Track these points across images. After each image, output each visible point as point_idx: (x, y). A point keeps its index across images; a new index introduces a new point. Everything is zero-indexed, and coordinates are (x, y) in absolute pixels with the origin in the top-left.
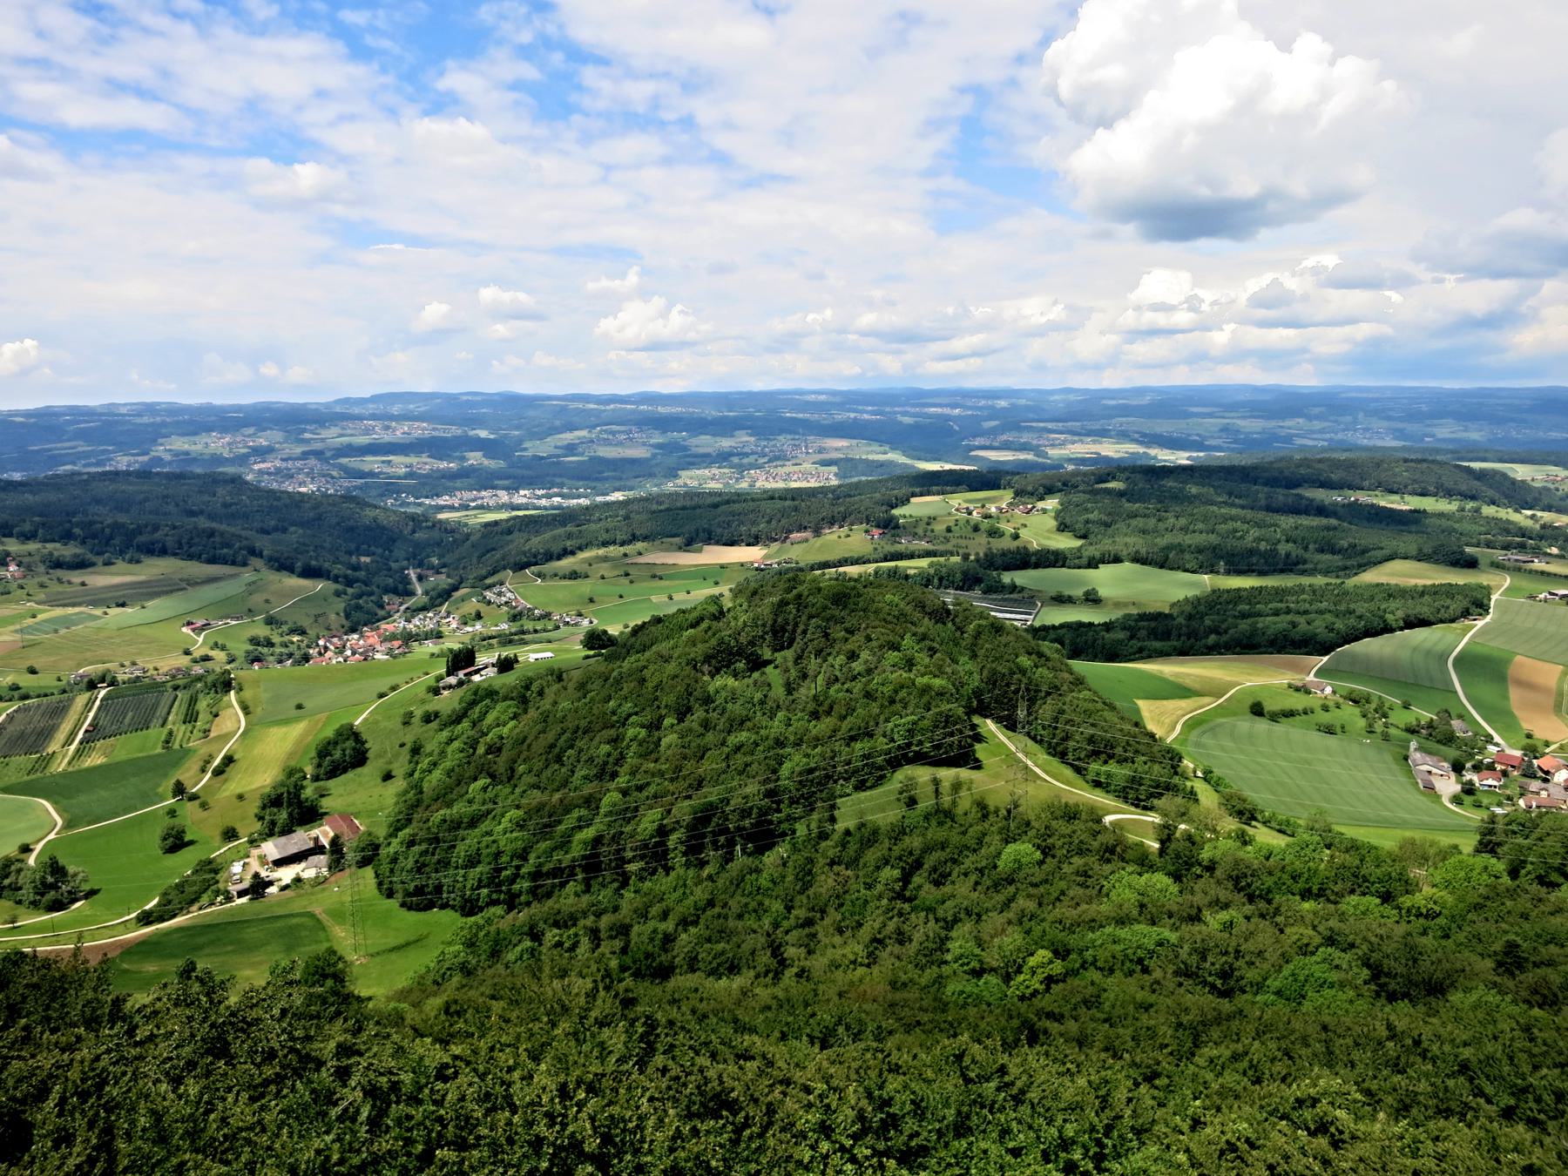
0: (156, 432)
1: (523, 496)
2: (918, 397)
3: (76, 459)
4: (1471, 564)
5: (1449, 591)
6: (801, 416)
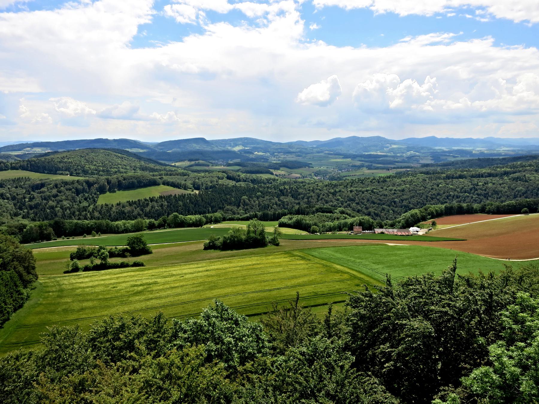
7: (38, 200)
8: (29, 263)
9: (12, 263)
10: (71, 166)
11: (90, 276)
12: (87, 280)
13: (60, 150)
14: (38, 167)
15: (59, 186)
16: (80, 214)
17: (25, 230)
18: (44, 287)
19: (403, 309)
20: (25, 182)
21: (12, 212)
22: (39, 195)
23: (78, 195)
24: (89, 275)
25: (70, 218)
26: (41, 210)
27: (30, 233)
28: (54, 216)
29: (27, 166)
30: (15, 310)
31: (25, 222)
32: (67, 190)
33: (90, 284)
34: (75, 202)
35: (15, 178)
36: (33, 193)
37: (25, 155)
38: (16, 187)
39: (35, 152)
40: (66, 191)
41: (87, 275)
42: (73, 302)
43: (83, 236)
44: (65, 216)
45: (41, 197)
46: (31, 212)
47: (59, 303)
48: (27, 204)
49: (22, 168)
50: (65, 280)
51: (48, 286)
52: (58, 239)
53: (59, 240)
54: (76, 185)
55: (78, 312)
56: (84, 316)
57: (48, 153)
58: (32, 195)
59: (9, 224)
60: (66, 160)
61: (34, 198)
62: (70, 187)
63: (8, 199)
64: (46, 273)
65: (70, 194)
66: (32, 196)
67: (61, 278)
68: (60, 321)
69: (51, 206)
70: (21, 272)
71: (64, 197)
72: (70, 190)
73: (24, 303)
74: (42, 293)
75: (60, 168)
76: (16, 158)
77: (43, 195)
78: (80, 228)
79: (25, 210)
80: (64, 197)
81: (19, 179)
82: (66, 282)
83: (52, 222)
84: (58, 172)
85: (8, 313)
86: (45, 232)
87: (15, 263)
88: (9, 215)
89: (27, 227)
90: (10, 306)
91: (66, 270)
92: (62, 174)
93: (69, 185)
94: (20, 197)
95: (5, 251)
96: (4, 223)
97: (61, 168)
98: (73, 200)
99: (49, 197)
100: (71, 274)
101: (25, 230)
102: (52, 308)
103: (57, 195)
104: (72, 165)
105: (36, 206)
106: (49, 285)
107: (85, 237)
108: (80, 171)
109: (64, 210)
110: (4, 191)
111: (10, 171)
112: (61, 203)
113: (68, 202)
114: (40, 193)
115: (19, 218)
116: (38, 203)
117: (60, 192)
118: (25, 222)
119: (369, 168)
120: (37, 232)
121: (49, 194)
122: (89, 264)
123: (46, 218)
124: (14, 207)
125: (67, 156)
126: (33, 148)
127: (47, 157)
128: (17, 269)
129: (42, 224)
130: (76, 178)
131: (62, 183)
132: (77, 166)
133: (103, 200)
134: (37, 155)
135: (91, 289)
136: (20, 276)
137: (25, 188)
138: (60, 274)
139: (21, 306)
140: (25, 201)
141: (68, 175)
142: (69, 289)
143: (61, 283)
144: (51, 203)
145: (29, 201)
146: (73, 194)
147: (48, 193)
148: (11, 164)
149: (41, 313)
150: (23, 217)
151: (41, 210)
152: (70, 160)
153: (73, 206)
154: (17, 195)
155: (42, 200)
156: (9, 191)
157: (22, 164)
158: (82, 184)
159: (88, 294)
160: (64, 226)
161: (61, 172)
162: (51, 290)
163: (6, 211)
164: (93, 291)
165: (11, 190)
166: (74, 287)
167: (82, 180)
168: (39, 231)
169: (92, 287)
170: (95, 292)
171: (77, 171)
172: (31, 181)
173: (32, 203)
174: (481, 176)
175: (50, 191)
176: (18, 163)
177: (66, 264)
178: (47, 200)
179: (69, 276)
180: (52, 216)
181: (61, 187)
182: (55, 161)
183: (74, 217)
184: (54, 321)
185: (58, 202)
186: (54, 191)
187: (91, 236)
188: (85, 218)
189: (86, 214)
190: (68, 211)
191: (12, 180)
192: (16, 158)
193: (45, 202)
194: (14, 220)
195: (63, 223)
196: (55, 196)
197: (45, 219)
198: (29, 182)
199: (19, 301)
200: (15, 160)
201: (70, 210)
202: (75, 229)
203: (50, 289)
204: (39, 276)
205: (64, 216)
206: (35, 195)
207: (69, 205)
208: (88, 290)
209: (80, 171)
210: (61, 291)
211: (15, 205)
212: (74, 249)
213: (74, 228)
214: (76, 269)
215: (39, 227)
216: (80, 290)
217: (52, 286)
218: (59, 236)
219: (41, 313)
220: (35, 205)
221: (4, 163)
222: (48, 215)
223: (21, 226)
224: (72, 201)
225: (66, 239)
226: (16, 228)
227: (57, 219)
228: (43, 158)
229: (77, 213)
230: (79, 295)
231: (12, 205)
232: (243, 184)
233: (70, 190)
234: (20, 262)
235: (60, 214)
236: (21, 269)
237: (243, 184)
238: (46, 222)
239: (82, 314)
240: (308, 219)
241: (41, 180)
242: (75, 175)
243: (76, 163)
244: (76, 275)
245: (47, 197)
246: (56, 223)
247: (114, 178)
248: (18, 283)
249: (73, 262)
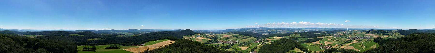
0: (248, 30)
1: (267, 33)
2: (291, 28)
3: (244, 31)
4: (322, 37)
5: (321, 38)
6: (39, 36)
31: (77, 42)
83: (81, 42)
118: (77, 42)
119: (135, 34)
133: (89, 40)
174: (152, 35)
212: (84, 47)
232: (112, 38)
237: (112, 38)
238: (80, 42)
240: (124, 44)
247: (90, 36)
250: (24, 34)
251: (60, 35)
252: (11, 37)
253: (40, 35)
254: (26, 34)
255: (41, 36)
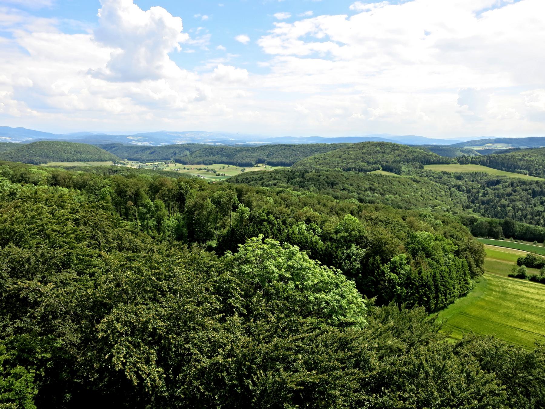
6: (255, 169)
7: (490, 197)
8: (480, 256)
9: (465, 252)
10: (532, 165)
11: (538, 289)
12: (533, 291)
13: (522, 147)
14: (497, 163)
15: (515, 185)
16: (532, 219)
17: (475, 223)
18: (488, 283)
19: (154, 220)
20: (482, 177)
21: (464, 204)
22: (493, 192)
23: (533, 198)
24: (537, 287)
25: (521, 220)
26: (492, 207)
27: (479, 228)
28: (504, 215)
29: (486, 161)
30: (460, 296)
32: (523, 190)
33: (537, 297)
34: (529, 204)
35: (473, 173)
36: (487, 189)
37: (486, 151)
38: (473, 181)
39: (496, 148)
40: (521, 191)
41: (533, 286)
42: (516, 309)
43: (532, 243)
44: (516, 217)
45: (495, 194)
46: (482, 207)
47: (501, 305)
48: (479, 198)
49: (482, 163)
50: (509, 283)
51: (491, 284)
52: (505, 239)
53: (507, 240)
54: (534, 186)
55: (519, 321)
56: (525, 328)
57: (509, 149)
58: (486, 190)
59: (461, 215)
60: (527, 158)
61: (487, 194)
62: (527, 187)
63: (463, 191)
64: (490, 271)
65: (525, 195)
66: (486, 192)
67: (506, 281)
68: (500, 323)
69: (503, 204)
70: (471, 263)
71: (518, 197)
72: (527, 190)
73: (468, 293)
74: (485, 289)
75: (519, 166)
76: (477, 153)
77: (496, 191)
78: (531, 233)
79: (477, 205)
80: (518, 197)
81: (476, 173)
82: (509, 285)
83: (502, 221)
84: (517, 170)
85: (454, 296)
86: (494, 230)
87: (468, 253)
88: (461, 206)
89: (478, 221)
90: (457, 292)
91: (511, 273)
92: (520, 173)
93: (526, 185)
94: (475, 191)
95: (461, 239)
96: (457, 213)
97: (521, 165)
98: (528, 201)
99: (503, 194)
100: (516, 279)
101: (475, 223)
102: (494, 307)
103: (511, 194)
104: (533, 164)
105: (488, 202)
106: (492, 283)
107: (535, 244)
108: (541, 172)
109: (516, 211)
110: (461, 183)
111: (469, 165)
112: (513, 203)
113: (522, 203)
114: (495, 189)
115: (471, 210)
116: (490, 199)
117: (515, 191)
118: (476, 216)
120: (486, 228)
121: (503, 191)
122: (537, 274)
123: (496, 216)
124: (467, 200)
125: (529, 154)
126: (494, 144)
127: (508, 154)
128: (468, 259)
129: (492, 221)
130: (536, 179)
131: (519, 182)
132: (539, 166)
134: (497, 151)
135: (537, 302)
136: (470, 266)
137: (481, 183)
138: (505, 276)
139: (465, 295)
140: (478, 195)
141: (526, 174)
142: (512, 294)
143: (505, 285)
144: (503, 201)
145: (482, 196)
146: (529, 196)
147: (502, 191)
148: (472, 158)
149: (482, 308)
150: (474, 211)
151: (492, 207)
152: (532, 159)
153: (526, 208)
154: (472, 188)
155: (495, 197)
156: (466, 184)
157: (482, 158)
158: (542, 186)
159: (533, 307)
160: (514, 227)
161: (520, 170)
162: (495, 289)
163: (460, 202)
164: (539, 305)
165: (467, 183)
166: (518, 294)
167: (541, 181)
168: (488, 227)
169: (538, 300)
170: (541, 308)
171: (538, 171)
172: (488, 176)
173: (485, 199)
175: (505, 189)
176: (478, 158)
177: (513, 267)
178: (500, 198)
179: (513, 281)
180: (502, 214)
181: (517, 186)
182: (515, 158)
183: (526, 220)
184: (494, 321)
185: (511, 202)
186: (509, 190)
187: (542, 244)
188: (537, 223)
189: (539, 219)
190: (520, 212)
191: (470, 174)
192: (477, 153)
193: (497, 199)
194: (465, 212)
195: (513, 224)
196: (510, 195)
197: (494, 216)
198: (486, 178)
199: (465, 289)
200: (476, 155)
201: (522, 212)
202: (525, 233)
203: (493, 288)
204: (485, 272)
205: (514, 217)
206: (489, 192)
207: (521, 207)
208: (533, 302)
209: (541, 172)
210: (505, 293)
211: (469, 198)
212: (523, 254)
213: (524, 231)
214: (522, 276)
215: (490, 223)
216: (525, 299)
217: (495, 286)
218: (507, 237)
219: (482, 308)
220: (487, 201)
221: (466, 157)
222: (498, 213)
223: (472, 219)
224: (527, 203)
225: (513, 241)
226: (467, 220)
227: (507, 218)
228: (503, 154)
229: (529, 216)
230: (523, 304)
231: (466, 198)
233: (527, 190)
234: (472, 253)
235: (510, 214)
236: (472, 260)
238: (497, 220)
239: (524, 325)
241: (498, 176)
242: (535, 175)
243: (538, 162)
244: (522, 282)
245: (500, 194)
246: (507, 223)
248: (467, 272)
249: (520, 268)
250: (166, 159)
251: (369, 167)
252: (81, 186)
253: (262, 168)
254: (177, 157)
255: (264, 173)
